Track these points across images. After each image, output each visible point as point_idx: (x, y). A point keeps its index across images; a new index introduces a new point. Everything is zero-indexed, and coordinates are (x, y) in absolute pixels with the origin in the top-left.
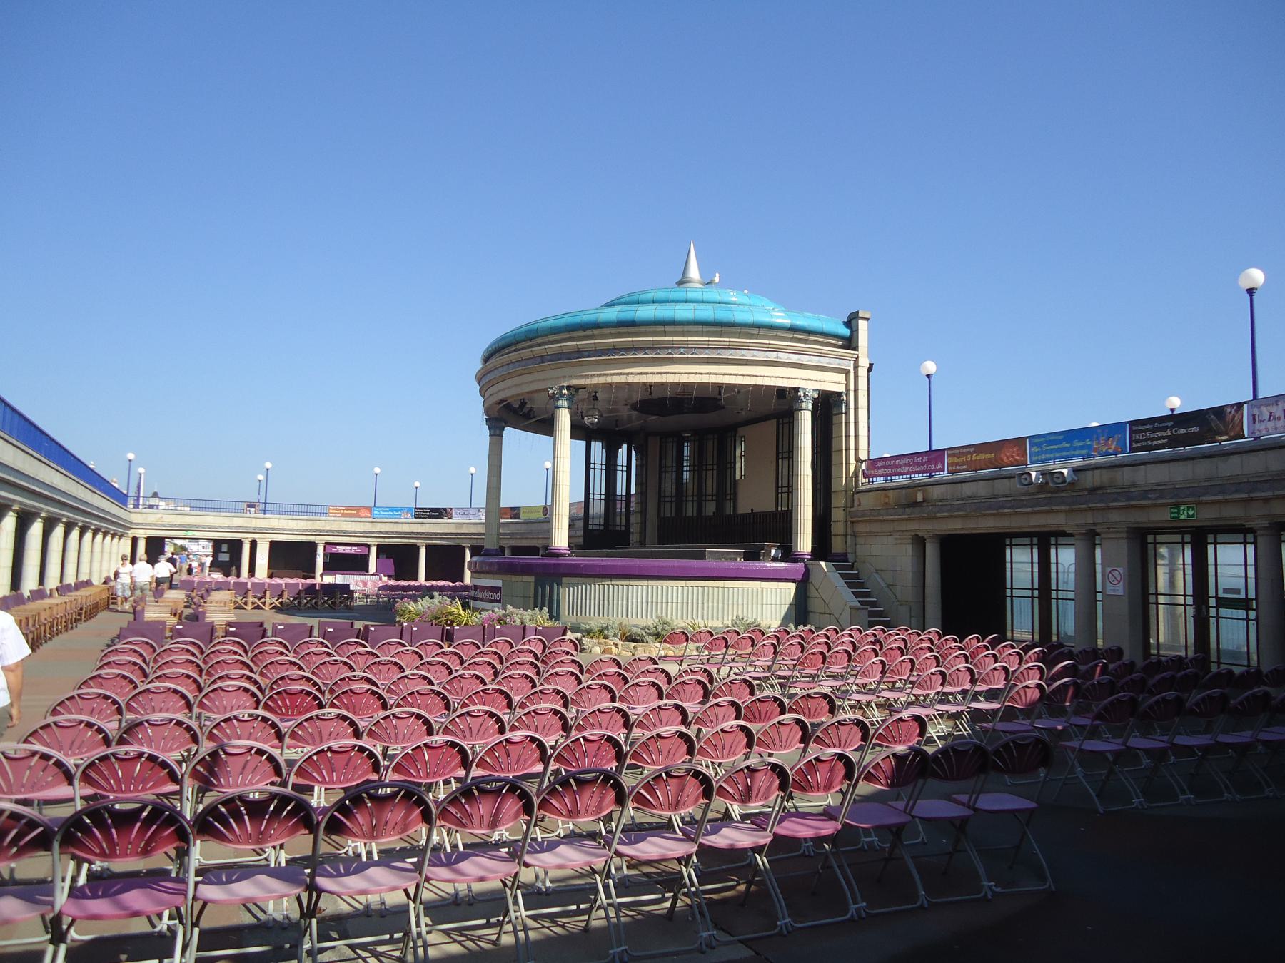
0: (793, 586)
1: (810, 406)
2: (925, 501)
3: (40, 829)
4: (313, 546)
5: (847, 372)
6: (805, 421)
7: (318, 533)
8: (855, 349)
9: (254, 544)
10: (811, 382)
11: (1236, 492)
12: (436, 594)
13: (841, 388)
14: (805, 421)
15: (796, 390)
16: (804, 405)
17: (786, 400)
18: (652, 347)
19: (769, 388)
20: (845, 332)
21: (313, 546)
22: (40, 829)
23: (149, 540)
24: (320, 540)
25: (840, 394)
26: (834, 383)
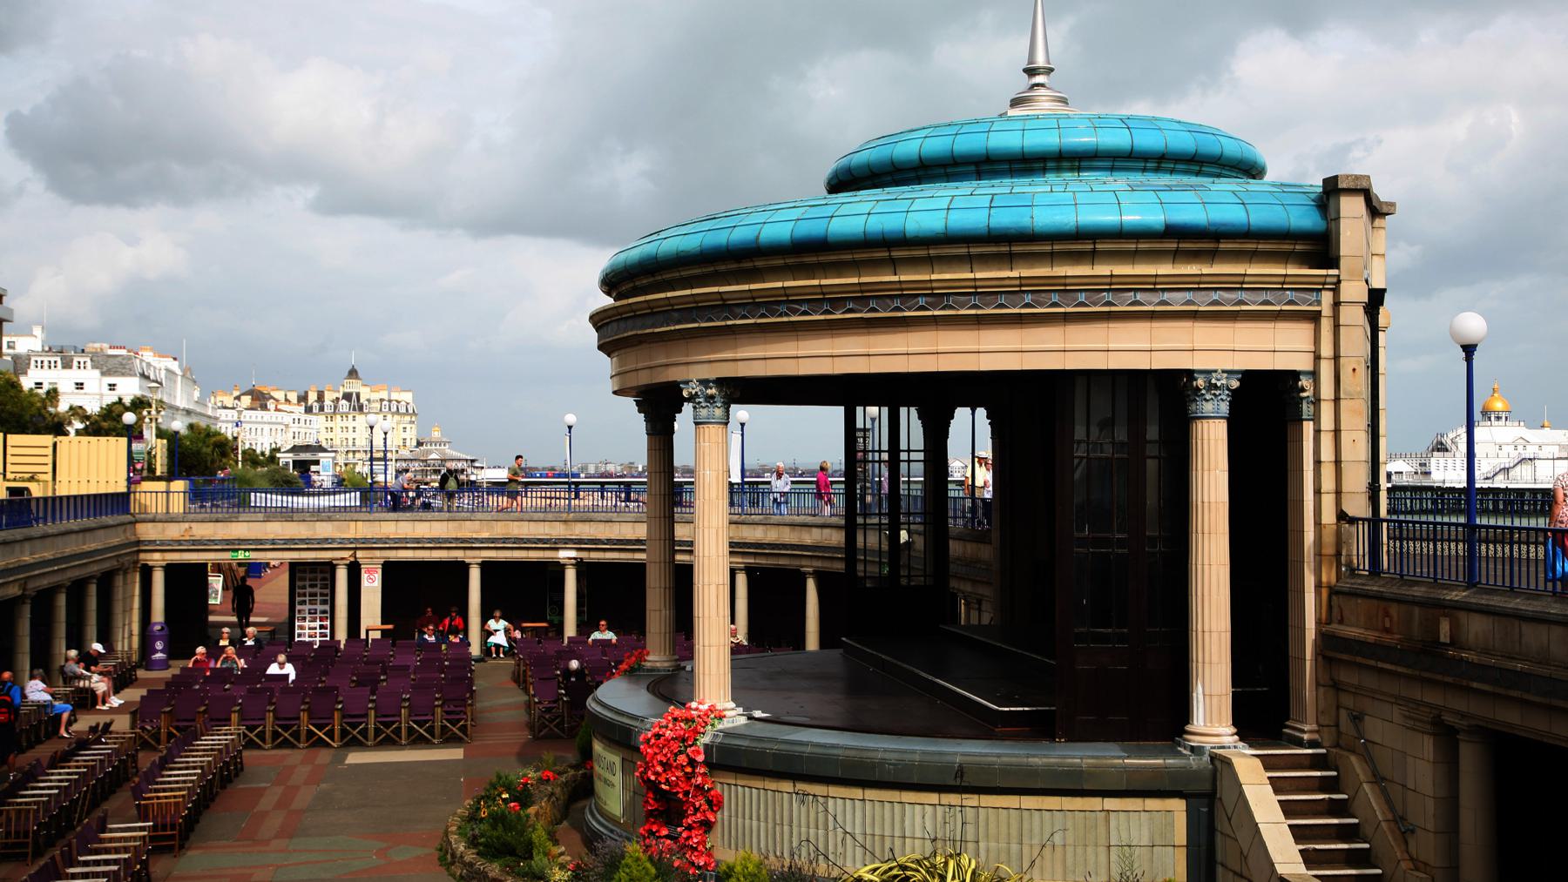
0: (1178, 806)
1: (1224, 408)
2: (1454, 643)
3: (1366, 846)
4: (462, 568)
5: (1315, 317)
6: (1212, 442)
7: (466, 544)
8: (1332, 261)
9: (354, 571)
10: (1221, 350)
11: (1496, 512)
12: (328, 484)
13: (1302, 363)
14: (1212, 442)
15: (1190, 374)
16: (1208, 407)
17: (1172, 392)
18: (863, 297)
19: (733, 668)
20: (1304, 218)
21: (462, 568)
22: (1366, 846)
23: (171, 570)
24: (474, 558)
25: (1295, 375)
26: (1278, 347)
